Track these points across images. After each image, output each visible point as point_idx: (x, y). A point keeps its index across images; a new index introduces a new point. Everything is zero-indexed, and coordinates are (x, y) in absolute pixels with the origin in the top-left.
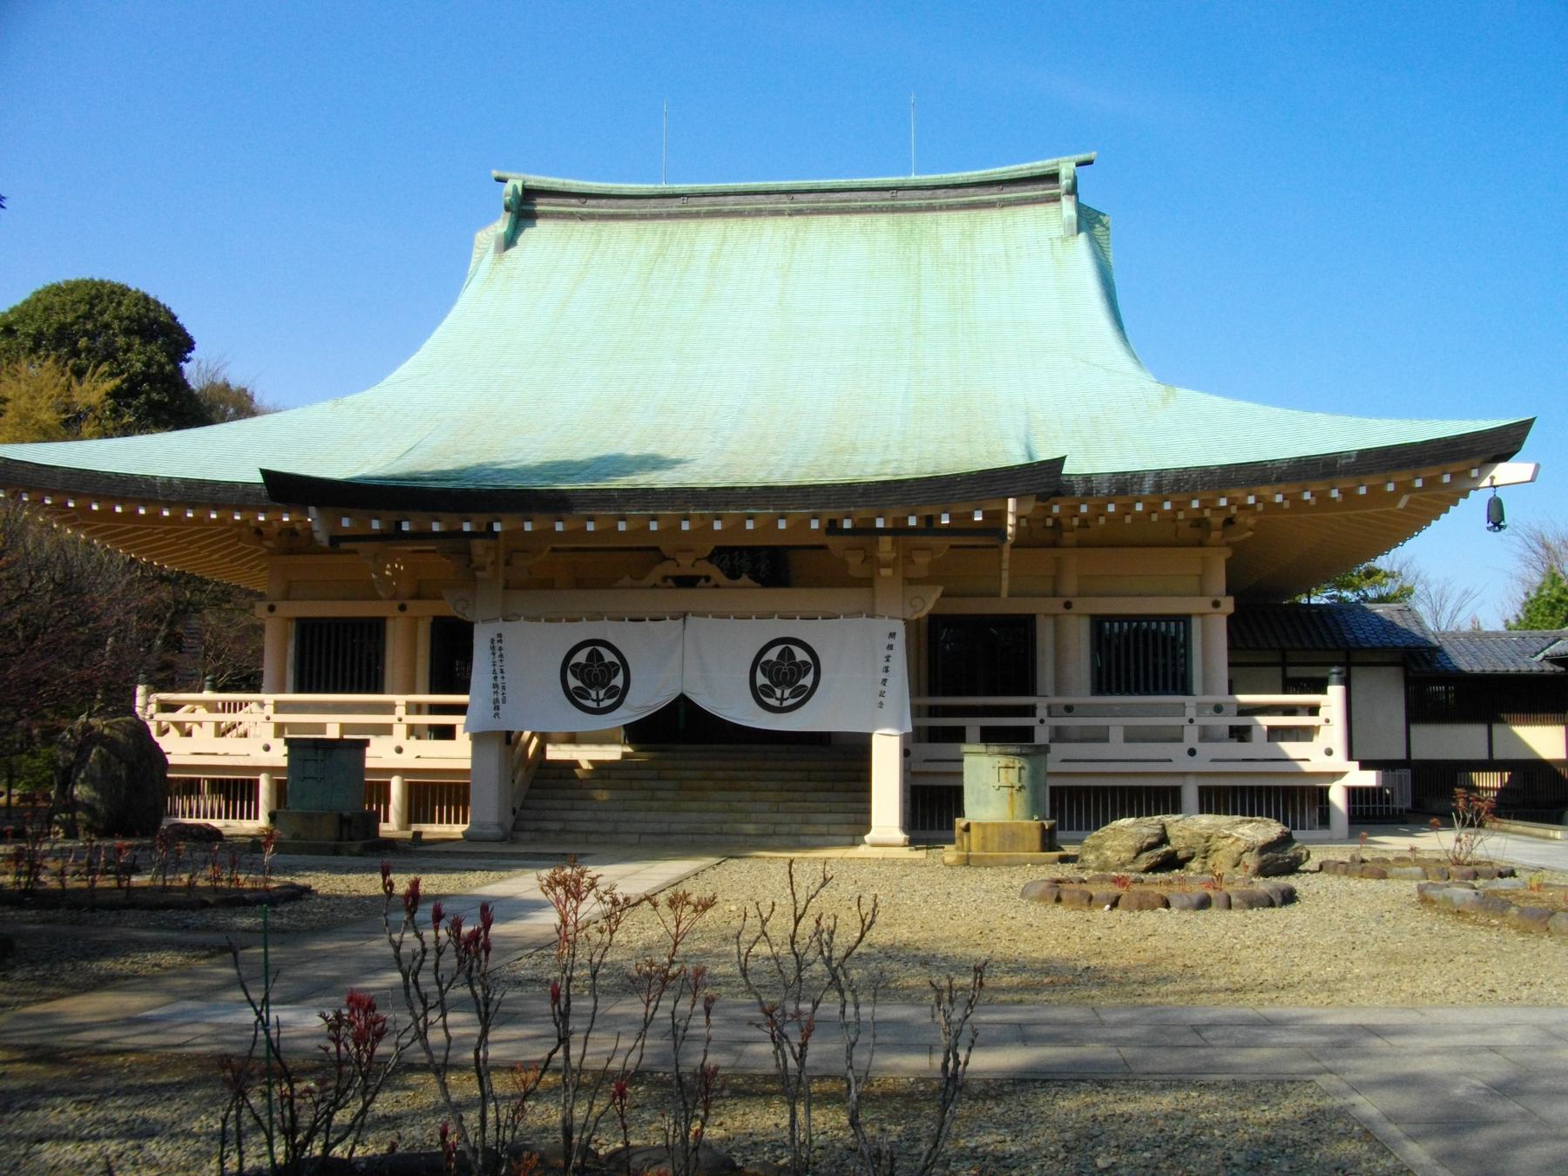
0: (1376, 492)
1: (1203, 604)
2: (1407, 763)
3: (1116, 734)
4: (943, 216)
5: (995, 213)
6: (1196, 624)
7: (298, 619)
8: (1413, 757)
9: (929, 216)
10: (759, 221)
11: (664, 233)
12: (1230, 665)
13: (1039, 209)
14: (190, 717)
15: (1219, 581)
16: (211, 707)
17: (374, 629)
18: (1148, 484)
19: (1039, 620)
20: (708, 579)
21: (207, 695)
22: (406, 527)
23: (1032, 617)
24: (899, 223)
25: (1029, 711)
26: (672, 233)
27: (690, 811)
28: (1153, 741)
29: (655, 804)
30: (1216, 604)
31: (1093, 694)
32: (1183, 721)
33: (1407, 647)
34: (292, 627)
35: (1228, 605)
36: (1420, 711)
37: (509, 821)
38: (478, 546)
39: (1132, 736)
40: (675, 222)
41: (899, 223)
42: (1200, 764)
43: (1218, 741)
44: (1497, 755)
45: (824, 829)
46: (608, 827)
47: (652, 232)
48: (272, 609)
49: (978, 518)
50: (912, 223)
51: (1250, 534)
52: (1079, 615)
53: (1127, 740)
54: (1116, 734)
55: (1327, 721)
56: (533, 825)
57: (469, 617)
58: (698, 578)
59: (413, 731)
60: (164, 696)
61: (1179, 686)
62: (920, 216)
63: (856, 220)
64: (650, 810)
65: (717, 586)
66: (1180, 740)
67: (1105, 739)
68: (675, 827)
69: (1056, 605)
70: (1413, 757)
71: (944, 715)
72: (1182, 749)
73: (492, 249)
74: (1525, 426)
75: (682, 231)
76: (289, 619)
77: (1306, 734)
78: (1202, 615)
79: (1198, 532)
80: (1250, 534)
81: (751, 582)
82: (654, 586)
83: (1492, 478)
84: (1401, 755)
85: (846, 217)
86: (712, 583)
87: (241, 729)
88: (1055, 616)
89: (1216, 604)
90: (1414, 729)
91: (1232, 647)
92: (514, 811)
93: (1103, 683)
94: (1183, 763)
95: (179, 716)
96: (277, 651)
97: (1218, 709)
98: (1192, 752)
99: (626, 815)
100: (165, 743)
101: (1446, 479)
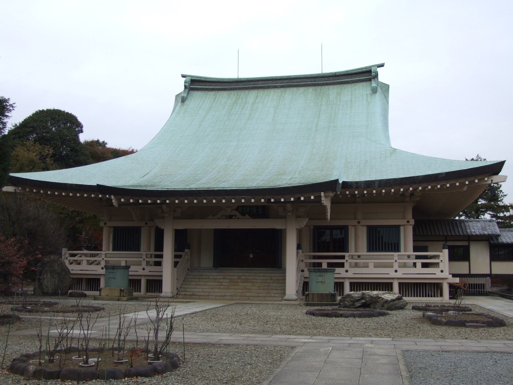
0: (453, 186)
1: (404, 222)
2: (490, 275)
3: (371, 265)
4: (331, 87)
5: (349, 86)
6: (402, 228)
7: (113, 227)
8: (492, 273)
9: (327, 87)
10: (269, 90)
11: (237, 95)
12: (414, 241)
13: (364, 84)
14: (80, 258)
15: (409, 215)
16: (86, 255)
17: (137, 231)
18: (376, 185)
19: (350, 227)
20: (235, 216)
21: (85, 252)
22: (140, 201)
23: (347, 226)
24: (316, 90)
25: (343, 257)
26: (240, 95)
27: (233, 289)
28: (387, 267)
29: (222, 287)
30: (408, 222)
31: (368, 252)
32: (394, 261)
33: (489, 235)
34: (112, 229)
35: (412, 222)
36: (494, 258)
37: (176, 292)
38: (164, 207)
39: (376, 266)
40: (242, 91)
41: (316, 90)
42: (399, 275)
43: (409, 267)
44: (472, 272)
45: (273, 295)
46: (207, 294)
47: (234, 94)
48: (105, 224)
49: (312, 197)
50: (321, 90)
51: (419, 198)
52: (363, 226)
53: (375, 267)
54: (371, 265)
55: (441, 261)
56: (184, 293)
57: (162, 228)
58: (232, 216)
59: (148, 263)
60: (72, 252)
61: (390, 249)
62: (323, 87)
63: (302, 89)
64: (220, 288)
65: (238, 218)
66: (392, 267)
67: (367, 267)
68: (227, 294)
69: (355, 222)
70: (492, 273)
71: (318, 259)
72: (141, 267)
73: (180, 102)
74: (502, 164)
75: (243, 94)
76: (111, 227)
77: (436, 265)
78: (404, 225)
79: (399, 199)
80: (419, 198)
81: (249, 217)
82: (219, 218)
83: (492, 180)
84: (488, 272)
85: (298, 88)
86: (237, 217)
87: (97, 262)
88: (355, 226)
89: (408, 222)
90: (493, 263)
91: (414, 235)
92: (177, 289)
93: (371, 248)
94: (393, 274)
95: (76, 258)
96: (107, 240)
97: (409, 257)
98: (347, 271)
99: (213, 290)
100: (70, 267)
101: (476, 181)
